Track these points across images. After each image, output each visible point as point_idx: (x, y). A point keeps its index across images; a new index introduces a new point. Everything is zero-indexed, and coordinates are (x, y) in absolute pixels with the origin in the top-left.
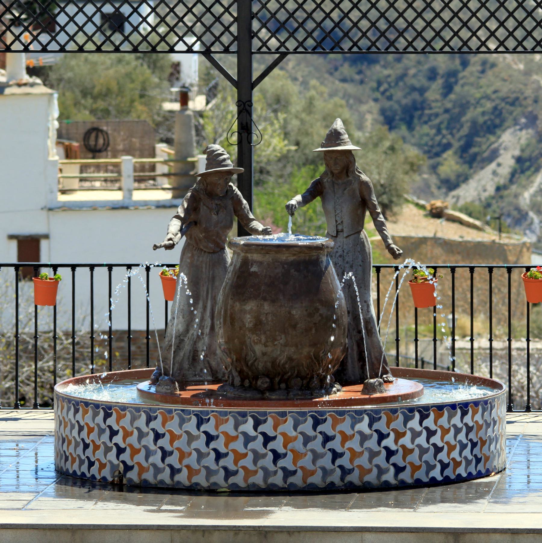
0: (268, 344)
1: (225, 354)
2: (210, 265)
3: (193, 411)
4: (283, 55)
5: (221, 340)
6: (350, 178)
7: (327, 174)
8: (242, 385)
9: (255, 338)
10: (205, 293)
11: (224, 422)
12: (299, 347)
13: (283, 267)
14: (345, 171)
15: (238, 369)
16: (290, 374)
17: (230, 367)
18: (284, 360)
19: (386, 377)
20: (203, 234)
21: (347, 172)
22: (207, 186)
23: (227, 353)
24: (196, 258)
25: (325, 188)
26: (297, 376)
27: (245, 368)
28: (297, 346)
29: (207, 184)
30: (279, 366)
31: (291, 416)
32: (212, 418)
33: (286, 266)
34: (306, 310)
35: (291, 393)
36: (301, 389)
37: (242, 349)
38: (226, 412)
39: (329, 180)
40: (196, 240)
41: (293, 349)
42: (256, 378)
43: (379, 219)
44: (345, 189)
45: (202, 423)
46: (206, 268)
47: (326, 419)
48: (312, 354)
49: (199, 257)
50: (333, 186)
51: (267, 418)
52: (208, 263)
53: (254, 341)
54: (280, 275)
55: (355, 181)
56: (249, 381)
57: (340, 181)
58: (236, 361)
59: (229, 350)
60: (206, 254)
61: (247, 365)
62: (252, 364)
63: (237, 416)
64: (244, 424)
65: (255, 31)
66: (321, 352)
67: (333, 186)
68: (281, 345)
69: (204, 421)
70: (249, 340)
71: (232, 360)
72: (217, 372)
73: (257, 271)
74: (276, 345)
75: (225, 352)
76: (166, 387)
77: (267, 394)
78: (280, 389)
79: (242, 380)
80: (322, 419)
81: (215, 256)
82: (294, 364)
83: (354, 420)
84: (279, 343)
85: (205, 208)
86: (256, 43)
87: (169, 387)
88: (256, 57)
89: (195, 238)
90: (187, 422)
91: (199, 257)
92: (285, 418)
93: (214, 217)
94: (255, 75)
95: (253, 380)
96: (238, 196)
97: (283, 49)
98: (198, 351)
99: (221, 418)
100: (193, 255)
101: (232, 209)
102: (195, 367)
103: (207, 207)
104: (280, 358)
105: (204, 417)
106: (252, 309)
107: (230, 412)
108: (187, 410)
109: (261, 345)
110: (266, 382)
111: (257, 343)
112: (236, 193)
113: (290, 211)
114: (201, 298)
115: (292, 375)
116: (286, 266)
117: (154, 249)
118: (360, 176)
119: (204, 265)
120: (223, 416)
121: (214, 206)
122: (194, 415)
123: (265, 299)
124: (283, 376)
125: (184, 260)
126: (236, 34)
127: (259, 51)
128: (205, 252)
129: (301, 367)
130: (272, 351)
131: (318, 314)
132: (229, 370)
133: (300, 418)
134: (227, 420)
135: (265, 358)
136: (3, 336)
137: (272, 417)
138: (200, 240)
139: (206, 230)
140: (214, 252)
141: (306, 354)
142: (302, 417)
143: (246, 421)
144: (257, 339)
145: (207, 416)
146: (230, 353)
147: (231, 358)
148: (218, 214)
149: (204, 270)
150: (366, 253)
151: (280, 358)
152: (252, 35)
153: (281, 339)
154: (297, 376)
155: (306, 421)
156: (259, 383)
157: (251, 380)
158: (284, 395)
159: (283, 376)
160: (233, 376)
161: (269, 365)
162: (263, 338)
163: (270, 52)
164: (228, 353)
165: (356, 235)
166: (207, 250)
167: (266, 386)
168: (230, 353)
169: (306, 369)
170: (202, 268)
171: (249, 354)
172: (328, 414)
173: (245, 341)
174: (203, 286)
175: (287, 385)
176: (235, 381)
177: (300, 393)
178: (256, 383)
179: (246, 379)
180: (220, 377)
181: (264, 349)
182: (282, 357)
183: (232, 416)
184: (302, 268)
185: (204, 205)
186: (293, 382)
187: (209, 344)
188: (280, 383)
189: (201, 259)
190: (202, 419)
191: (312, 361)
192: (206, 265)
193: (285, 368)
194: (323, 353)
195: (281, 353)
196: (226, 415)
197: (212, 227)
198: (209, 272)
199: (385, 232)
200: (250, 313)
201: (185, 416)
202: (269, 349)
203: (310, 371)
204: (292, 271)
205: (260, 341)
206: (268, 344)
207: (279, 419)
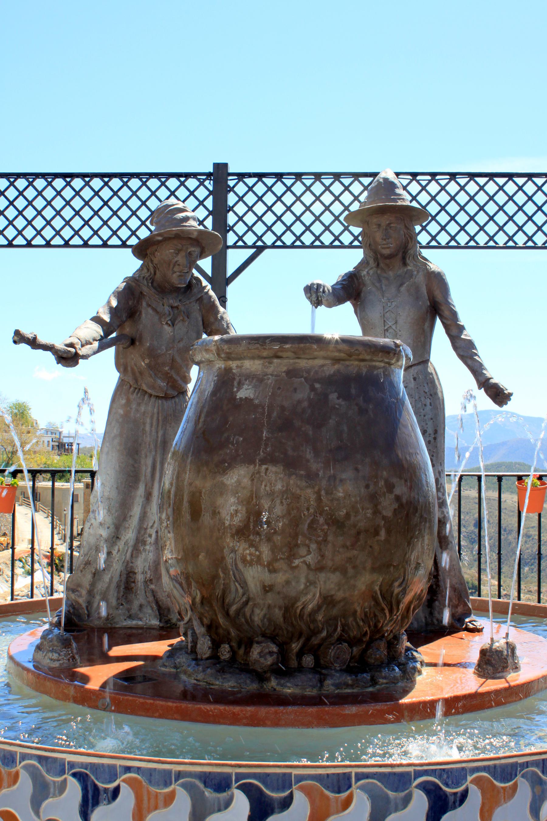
0: (277, 565)
1: (177, 586)
2: (158, 420)
3: (72, 765)
4: (260, 250)
5: (168, 555)
6: (409, 268)
7: (368, 263)
8: (215, 657)
9: (242, 548)
10: (149, 470)
11: (161, 803)
12: (351, 571)
13: (313, 389)
14: (400, 255)
15: (206, 621)
16: (324, 634)
17: (189, 613)
18: (315, 602)
19: (470, 622)
20: (147, 361)
21: (404, 259)
22: (155, 274)
23: (181, 584)
24: (134, 406)
25: (364, 285)
26: (340, 640)
27: (221, 620)
28: (344, 572)
29: (155, 268)
30: (301, 616)
31: (362, 788)
32: (126, 792)
33: (317, 386)
34: (367, 487)
35: (328, 682)
36: (349, 670)
37: (215, 577)
38: (168, 773)
39: (371, 272)
40: (133, 373)
41: (335, 577)
42: (249, 643)
43: (463, 337)
44: (402, 285)
45: (96, 803)
46: (151, 426)
47: (464, 795)
48: (377, 588)
49: (139, 404)
50: (380, 281)
51: (291, 794)
52: (156, 416)
53: (244, 560)
54: (305, 404)
55: (418, 272)
56: (231, 647)
57: (391, 273)
58: (202, 603)
59: (187, 577)
60: (153, 399)
61: (227, 614)
62: (239, 612)
63: (201, 786)
64: (219, 810)
65: (231, 225)
66: (396, 584)
67: (380, 281)
68: (309, 566)
69: (103, 796)
70: (232, 555)
71: (194, 600)
72: (169, 610)
73: (252, 396)
74: (297, 566)
75: (177, 581)
76: (50, 655)
77: (273, 683)
78: (300, 669)
79: (216, 645)
80: (455, 794)
81: (168, 404)
82: (335, 612)
83: (538, 789)
84: (304, 562)
85: (150, 311)
86: (231, 238)
87: (55, 656)
88: (230, 252)
89: (132, 369)
90: (54, 796)
91: (139, 404)
92: (344, 795)
93: (168, 329)
94: (230, 271)
95: (239, 647)
96: (210, 297)
97: (260, 243)
98: (135, 573)
99: (153, 789)
100: (128, 401)
101: (200, 319)
102: (129, 602)
103: (155, 310)
104: (303, 599)
105: (100, 785)
106: (239, 482)
107: (179, 775)
108: (55, 760)
109: (260, 568)
110: (271, 653)
111: (251, 563)
112: (207, 293)
113: (314, 296)
114: (143, 478)
115: (329, 636)
116: (317, 386)
117: (15, 342)
118: (427, 264)
119: (148, 420)
120: (158, 785)
121: (167, 309)
122: (74, 775)
123: (270, 459)
124: (308, 639)
125: (114, 411)
126: (211, 209)
127: (235, 246)
128: (151, 395)
129: (351, 619)
130: (288, 582)
131: (392, 496)
132: (186, 619)
133: (391, 794)
134: (170, 798)
135: (270, 599)
136: (2, 544)
137: (308, 792)
138: (141, 373)
139: (152, 353)
140: (166, 397)
141: (363, 588)
142: (396, 790)
143: (228, 804)
144: (251, 554)
145: (111, 782)
146: (189, 585)
147: (190, 594)
148: (173, 326)
149: (148, 428)
150: (439, 398)
151: (303, 599)
152: (228, 228)
153: (309, 553)
154: (340, 640)
155: (407, 800)
156: (255, 652)
157: (234, 644)
158: (313, 687)
159: (308, 639)
160: (194, 633)
161: (278, 614)
162: (265, 551)
163: (246, 246)
164: (185, 585)
165: (420, 367)
166: (154, 393)
167: (270, 660)
168: (189, 585)
169: (361, 623)
170: (144, 424)
171: (233, 589)
172: (469, 778)
173: (223, 558)
174: (146, 456)
175: (317, 660)
176: (199, 646)
177: (349, 679)
178: (247, 653)
179: (223, 642)
180: (174, 621)
181: (267, 578)
182: (309, 596)
183: (183, 786)
184: (353, 391)
185: (149, 305)
186: (332, 652)
187: (155, 561)
188: (300, 654)
189: (143, 409)
190: (96, 788)
191: (377, 603)
192: (152, 417)
193: (314, 621)
194: (400, 585)
195: (306, 587)
196: (167, 784)
197: (164, 347)
198: (157, 432)
199: (476, 357)
200: (235, 493)
201: (49, 778)
202: (280, 578)
203: (369, 627)
204: (333, 397)
205: (259, 558)
206: (277, 565)
207: (327, 798)
